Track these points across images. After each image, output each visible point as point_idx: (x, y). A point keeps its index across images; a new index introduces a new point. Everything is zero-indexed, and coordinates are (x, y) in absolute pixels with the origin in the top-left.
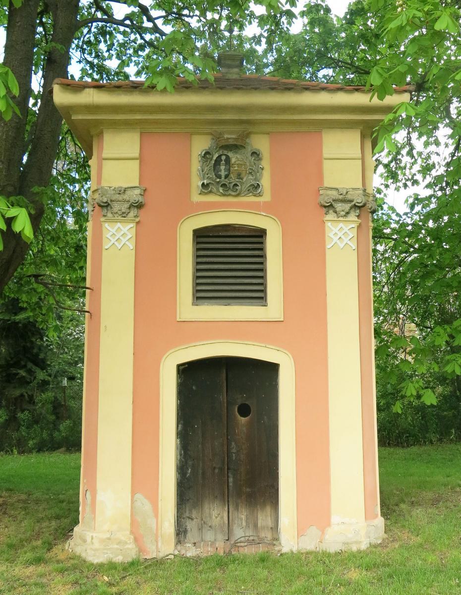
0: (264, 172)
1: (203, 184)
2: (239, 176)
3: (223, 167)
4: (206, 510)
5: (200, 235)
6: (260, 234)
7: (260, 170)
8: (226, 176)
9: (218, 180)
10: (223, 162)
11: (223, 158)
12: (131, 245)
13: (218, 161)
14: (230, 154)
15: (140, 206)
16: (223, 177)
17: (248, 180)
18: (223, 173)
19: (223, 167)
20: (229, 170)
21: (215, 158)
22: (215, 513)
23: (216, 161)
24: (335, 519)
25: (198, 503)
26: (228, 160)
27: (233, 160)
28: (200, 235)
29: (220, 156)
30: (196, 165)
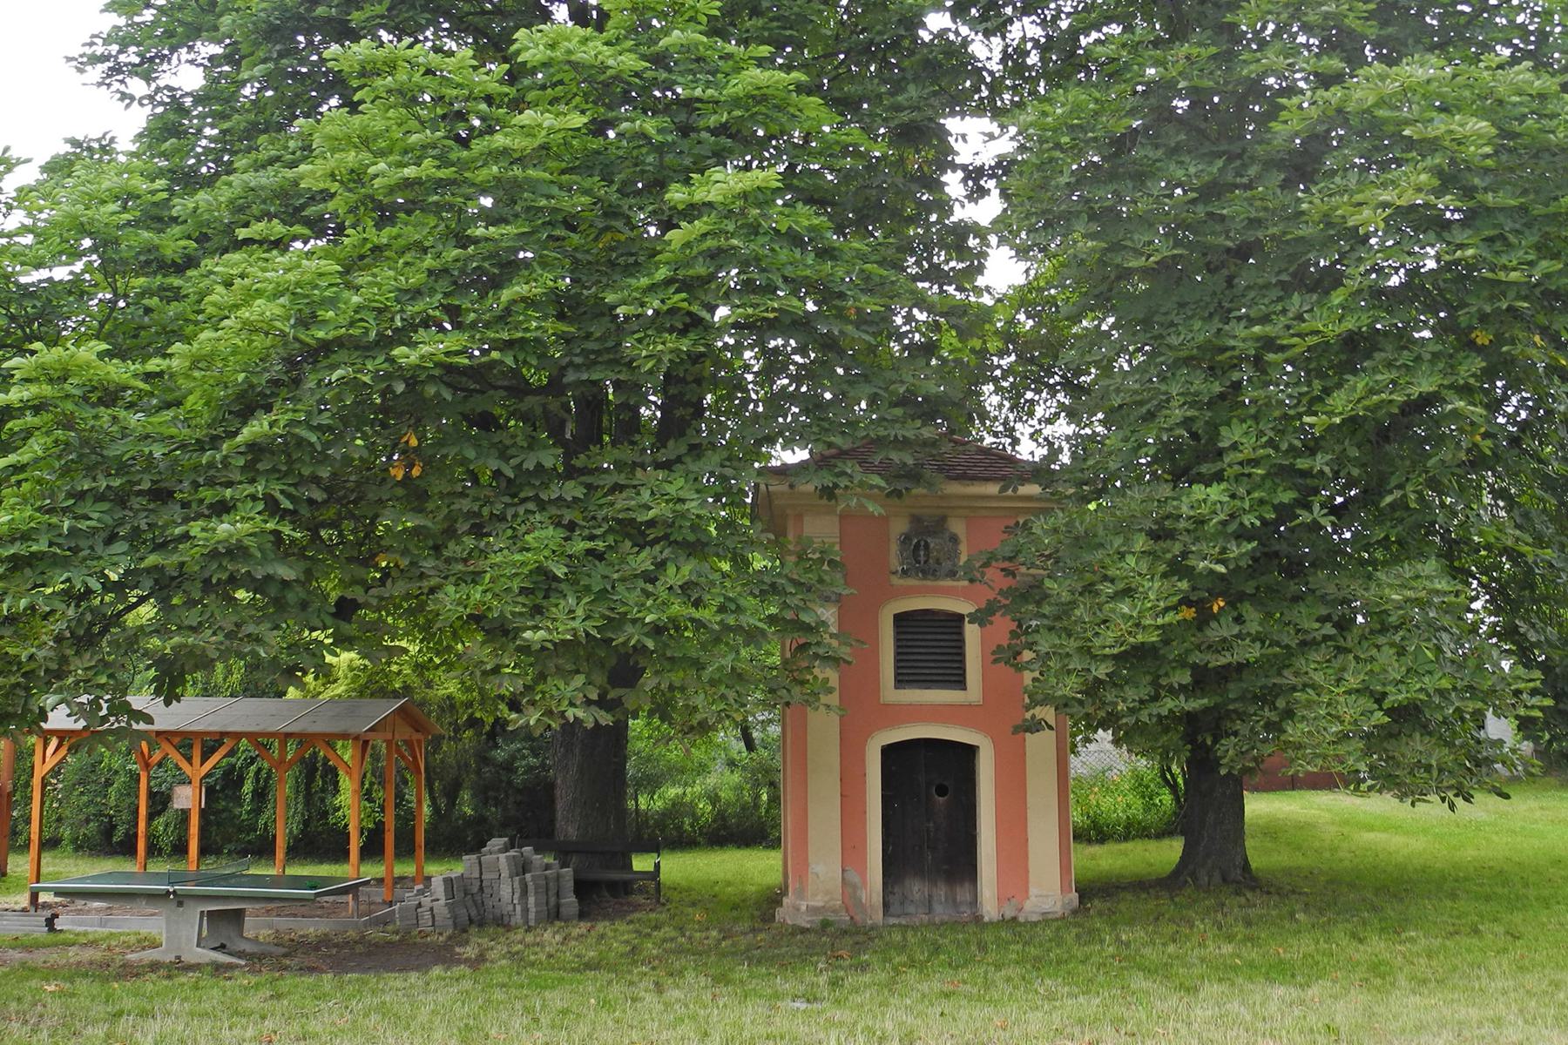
2: (938, 562)
5: (900, 619)
6: (970, 751)
13: (917, 546)
17: (947, 565)
18: (922, 559)
24: (1033, 891)
26: (927, 546)
28: (900, 619)
29: (918, 543)
30: (894, 548)
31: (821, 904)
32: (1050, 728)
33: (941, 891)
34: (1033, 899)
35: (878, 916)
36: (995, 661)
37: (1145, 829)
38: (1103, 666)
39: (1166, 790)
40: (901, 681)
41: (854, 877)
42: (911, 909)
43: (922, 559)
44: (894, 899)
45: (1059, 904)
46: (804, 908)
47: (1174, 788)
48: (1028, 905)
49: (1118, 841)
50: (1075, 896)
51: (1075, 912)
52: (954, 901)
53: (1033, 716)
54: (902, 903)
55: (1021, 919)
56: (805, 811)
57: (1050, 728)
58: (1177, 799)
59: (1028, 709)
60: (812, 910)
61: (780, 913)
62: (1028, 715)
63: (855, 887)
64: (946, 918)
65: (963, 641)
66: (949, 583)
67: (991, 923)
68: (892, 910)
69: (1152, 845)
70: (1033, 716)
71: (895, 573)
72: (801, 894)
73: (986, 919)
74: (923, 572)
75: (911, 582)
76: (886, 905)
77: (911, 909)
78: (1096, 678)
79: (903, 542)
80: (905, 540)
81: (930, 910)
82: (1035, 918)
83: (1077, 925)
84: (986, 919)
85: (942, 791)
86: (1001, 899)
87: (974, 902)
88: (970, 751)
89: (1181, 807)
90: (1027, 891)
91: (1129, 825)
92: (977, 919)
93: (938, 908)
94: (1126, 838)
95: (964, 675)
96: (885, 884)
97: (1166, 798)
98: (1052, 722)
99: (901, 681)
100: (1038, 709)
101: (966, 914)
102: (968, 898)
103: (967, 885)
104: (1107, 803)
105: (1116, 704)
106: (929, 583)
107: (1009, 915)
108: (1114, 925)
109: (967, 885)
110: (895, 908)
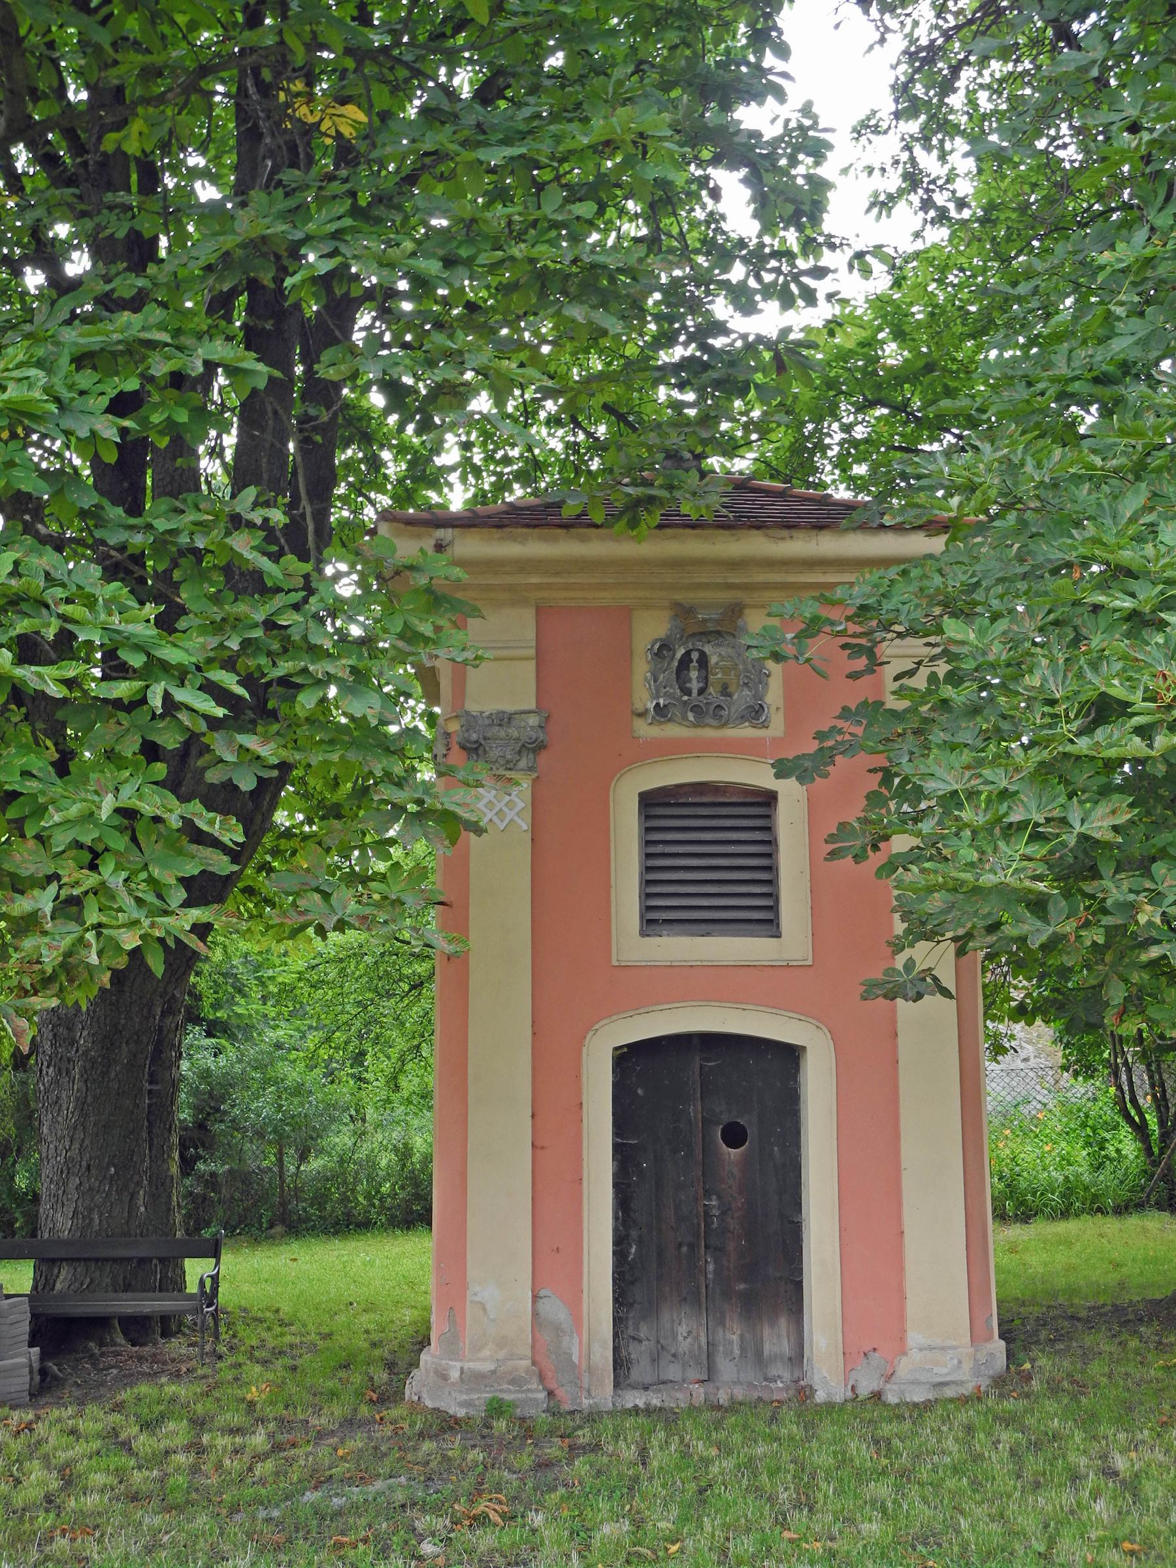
0: (771, 680)
1: (658, 704)
2: (725, 691)
3: (694, 674)
4: (666, 1316)
5: (650, 801)
6: (791, 1055)
7: (764, 679)
8: (701, 692)
9: (685, 698)
10: (695, 664)
11: (695, 656)
12: (525, 825)
13: (685, 662)
14: (708, 649)
15: (536, 747)
16: (695, 692)
17: (742, 697)
18: (695, 686)
19: (694, 674)
20: (706, 678)
21: (679, 655)
22: (682, 1330)
23: (681, 661)
24: (914, 1338)
25: (651, 1311)
26: (703, 661)
27: (713, 660)
28: (650, 801)
29: (688, 653)
30: (641, 668)
31: (488, 1366)
32: (945, 993)
33: (733, 1335)
34: (915, 1356)
35: (604, 1394)
36: (833, 855)
37: (1095, 1198)
38: (1103, 809)
39: (1125, 1130)
40: (651, 924)
41: (554, 1309)
42: (673, 1372)
43: (695, 686)
44: (638, 1353)
45: (967, 1365)
46: (455, 1375)
47: (1141, 1130)
48: (904, 1368)
49: (1052, 1218)
50: (999, 1346)
51: (999, 1382)
52: (759, 1353)
53: (910, 964)
54: (655, 1360)
55: (892, 1398)
56: (464, 1175)
57: (945, 993)
58: (1149, 1151)
59: (897, 947)
60: (472, 1379)
61: (418, 1386)
62: (900, 961)
63: (558, 1330)
64: (739, 1393)
65: (772, 843)
66: (746, 732)
67: (830, 1406)
68: (635, 1375)
69: (1111, 1225)
70: (910, 964)
71: (642, 715)
72: (453, 1349)
73: (820, 1396)
74: (696, 709)
75: (674, 731)
76: (620, 1364)
77: (673, 1372)
78: (1084, 838)
79: (658, 654)
80: (663, 649)
81: (710, 1375)
82: (918, 1396)
83: (1009, 1420)
84: (820, 1396)
85: (734, 1135)
86: (851, 1355)
87: (797, 1358)
88: (791, 1055)
89: (1155, 1164)
90: (902, 1339)
91: (1069, 1190)
92: (804, 1393)
93: (726, 1369)
94: (1065, 1214)
95: (774, 908)
96: (617, 1321)
97: (1128, 1145)
98: (949, 983)
99: (651, 924)
100: (923, 946)
101: (779, 1389)
102: (786, 1348)
103: (783, 1322)
104: (1028, 1154)
105: (1132, 908)
106: (709, 733)
107: (865, 1388)
108: (1089, 1421)
109: (783, 1322)
110: (641, 1371)
